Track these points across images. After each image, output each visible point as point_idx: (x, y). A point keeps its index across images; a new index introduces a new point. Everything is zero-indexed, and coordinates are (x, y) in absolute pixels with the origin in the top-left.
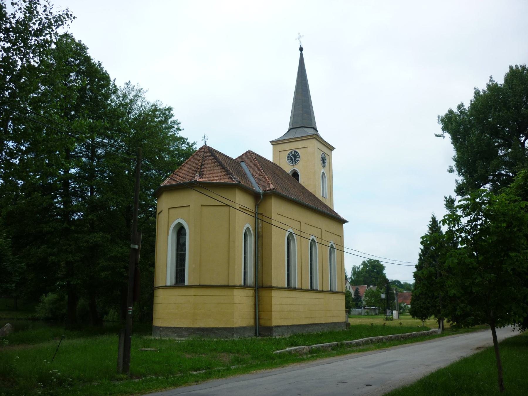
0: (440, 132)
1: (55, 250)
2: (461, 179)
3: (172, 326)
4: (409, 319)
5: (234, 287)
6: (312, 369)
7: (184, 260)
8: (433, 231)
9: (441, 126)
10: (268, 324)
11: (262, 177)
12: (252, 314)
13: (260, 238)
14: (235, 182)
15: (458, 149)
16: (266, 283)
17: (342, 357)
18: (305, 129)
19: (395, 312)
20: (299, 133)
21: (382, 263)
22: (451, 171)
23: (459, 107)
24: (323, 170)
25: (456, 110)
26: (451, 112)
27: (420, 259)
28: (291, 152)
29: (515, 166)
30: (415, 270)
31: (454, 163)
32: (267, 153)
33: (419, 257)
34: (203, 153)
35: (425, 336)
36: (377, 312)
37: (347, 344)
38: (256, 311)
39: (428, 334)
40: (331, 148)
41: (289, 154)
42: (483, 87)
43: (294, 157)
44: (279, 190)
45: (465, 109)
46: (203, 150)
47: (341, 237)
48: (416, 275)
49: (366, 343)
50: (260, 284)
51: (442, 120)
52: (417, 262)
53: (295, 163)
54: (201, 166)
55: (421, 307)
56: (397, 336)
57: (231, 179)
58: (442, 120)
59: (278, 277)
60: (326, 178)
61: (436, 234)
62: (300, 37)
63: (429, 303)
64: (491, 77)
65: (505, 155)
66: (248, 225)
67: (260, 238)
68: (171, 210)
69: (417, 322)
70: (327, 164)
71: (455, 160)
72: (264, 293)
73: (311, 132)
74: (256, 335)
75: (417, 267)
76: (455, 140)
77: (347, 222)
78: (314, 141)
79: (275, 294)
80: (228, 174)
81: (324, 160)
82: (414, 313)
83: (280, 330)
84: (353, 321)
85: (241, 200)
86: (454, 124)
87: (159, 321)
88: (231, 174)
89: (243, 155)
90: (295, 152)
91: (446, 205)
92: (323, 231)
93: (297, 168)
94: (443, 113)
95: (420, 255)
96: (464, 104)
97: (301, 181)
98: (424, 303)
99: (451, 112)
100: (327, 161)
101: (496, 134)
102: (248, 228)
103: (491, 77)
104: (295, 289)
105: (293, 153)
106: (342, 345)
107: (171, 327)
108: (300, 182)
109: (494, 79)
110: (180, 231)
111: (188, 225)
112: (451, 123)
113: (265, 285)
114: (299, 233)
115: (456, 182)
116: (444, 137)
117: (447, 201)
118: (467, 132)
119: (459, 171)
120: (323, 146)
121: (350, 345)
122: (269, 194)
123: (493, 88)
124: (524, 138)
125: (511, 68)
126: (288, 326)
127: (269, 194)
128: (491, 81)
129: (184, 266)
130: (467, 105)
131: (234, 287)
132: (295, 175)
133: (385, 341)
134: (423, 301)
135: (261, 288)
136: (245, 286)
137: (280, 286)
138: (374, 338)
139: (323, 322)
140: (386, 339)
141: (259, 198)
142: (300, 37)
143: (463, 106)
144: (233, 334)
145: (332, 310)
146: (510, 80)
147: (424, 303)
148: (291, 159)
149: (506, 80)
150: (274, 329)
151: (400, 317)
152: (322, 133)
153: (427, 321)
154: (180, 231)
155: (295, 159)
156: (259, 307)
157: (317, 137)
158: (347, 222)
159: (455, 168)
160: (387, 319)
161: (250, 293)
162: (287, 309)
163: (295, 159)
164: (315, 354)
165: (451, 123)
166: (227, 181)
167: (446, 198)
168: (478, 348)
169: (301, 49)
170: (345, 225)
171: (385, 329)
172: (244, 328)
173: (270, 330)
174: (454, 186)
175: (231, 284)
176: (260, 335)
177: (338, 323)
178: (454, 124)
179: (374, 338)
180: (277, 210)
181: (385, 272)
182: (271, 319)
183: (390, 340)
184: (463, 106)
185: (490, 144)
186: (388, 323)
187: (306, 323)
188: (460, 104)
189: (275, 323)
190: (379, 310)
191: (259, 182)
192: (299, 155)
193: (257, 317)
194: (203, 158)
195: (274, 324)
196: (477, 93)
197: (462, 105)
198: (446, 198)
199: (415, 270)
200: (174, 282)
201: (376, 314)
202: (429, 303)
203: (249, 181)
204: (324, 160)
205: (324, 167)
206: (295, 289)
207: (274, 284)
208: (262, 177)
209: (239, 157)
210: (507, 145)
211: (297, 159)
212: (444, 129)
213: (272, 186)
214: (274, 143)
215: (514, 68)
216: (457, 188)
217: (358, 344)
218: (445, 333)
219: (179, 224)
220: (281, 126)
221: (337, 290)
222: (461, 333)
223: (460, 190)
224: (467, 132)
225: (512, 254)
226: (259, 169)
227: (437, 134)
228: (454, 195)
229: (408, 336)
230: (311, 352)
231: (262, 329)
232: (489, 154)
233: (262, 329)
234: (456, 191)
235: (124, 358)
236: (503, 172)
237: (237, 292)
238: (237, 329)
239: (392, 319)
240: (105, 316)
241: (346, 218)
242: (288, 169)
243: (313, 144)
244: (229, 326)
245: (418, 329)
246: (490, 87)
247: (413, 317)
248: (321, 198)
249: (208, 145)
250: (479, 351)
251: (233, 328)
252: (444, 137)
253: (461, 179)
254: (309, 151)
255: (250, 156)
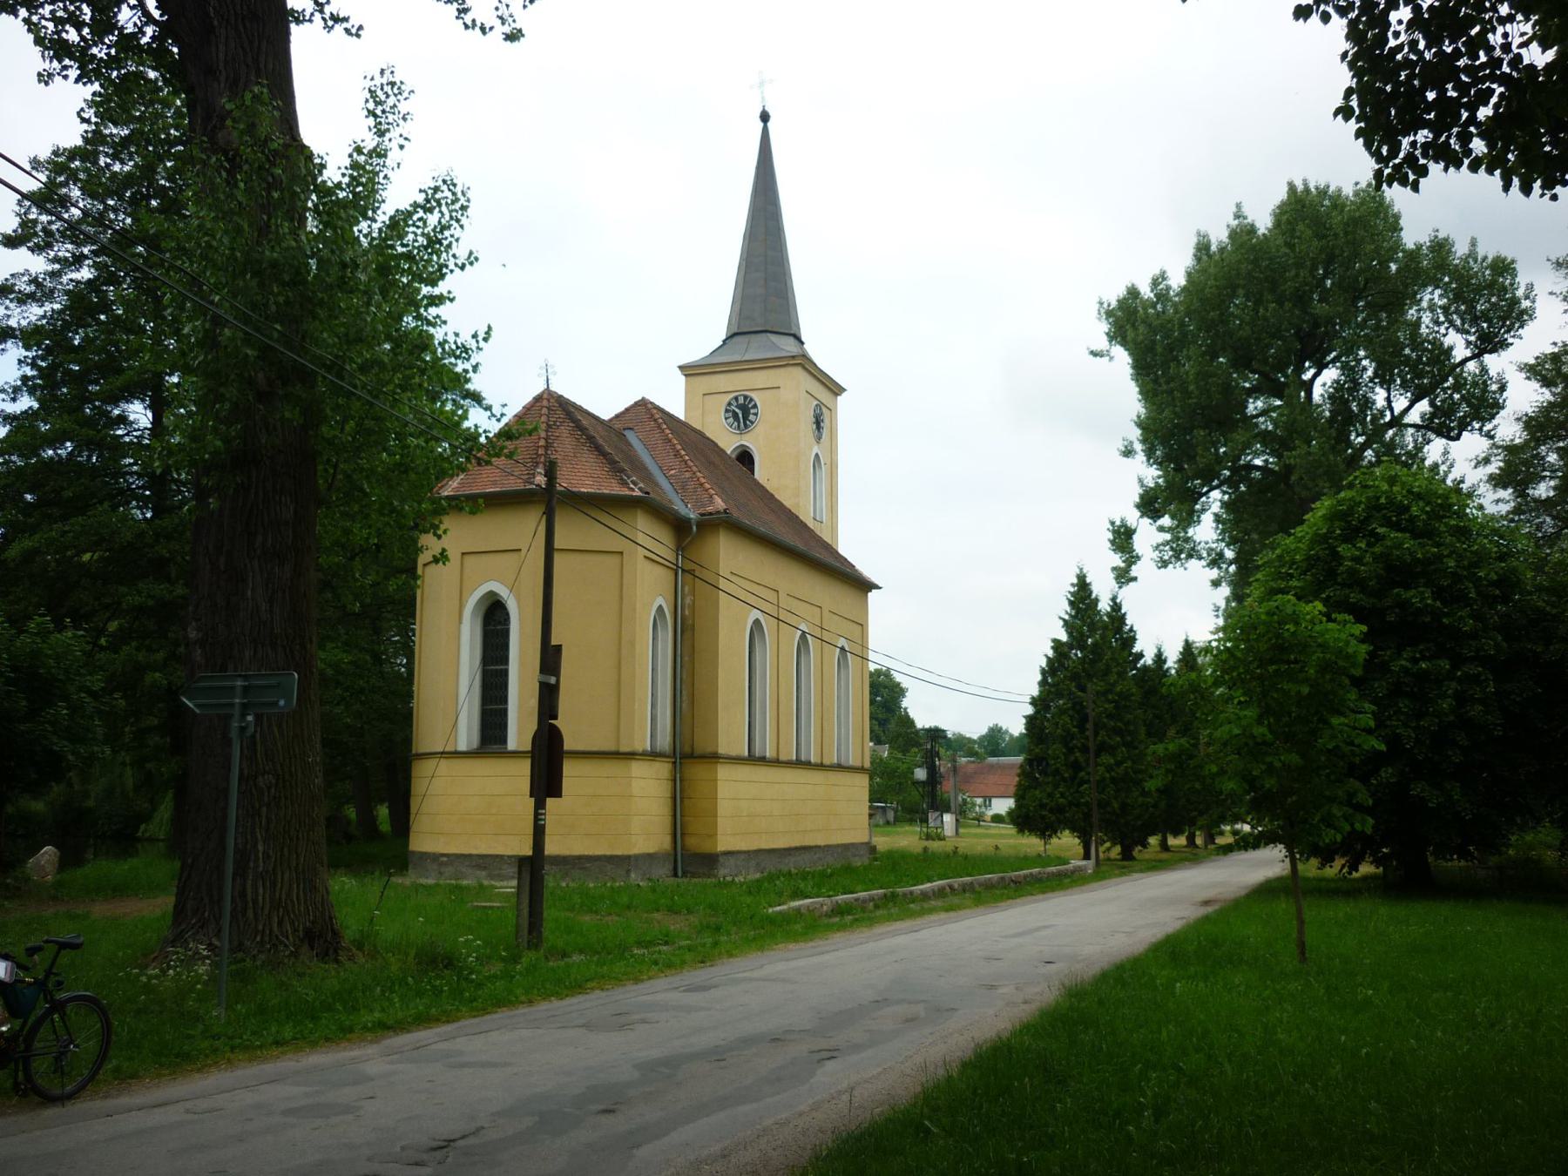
0: (1102, 343)
1: (160, 656)
2: (1153, 475)
3: (474, 852)
4: (1011, 836)
5: (631, 756)
6: (885, 943)
7: (504, 686)
8: (1078, 610)
9: (1104, 327)
10: (706, 847)
11: (688, 475)
12: (668, 820)
13: (689, 635)
14: (637, 493)
15: (1147, 394)
16: (702, 746)
17: (981, 909)
18: (773, 338)
19: (947, 818)
20: (755, 349)
21: (898, 678)
22: (1128, 453)
23: (1155, 283)
24: (816, 450)
25: (1146, 292)
26: (1133, 292)
27: (1043, 683)
28: (736, 398)
29: (1290, 449)
30: (1030, 710)
31: (1136, 433)
32: (673, 399)
33: (1039, 677)
34: (545, 411)
35: (1059, 880)
36: (891, 815)
37: (905, 895)
38: (675, 816)
39: (1060, 876)
40: (836, 389)
41: (729, 404)
42: (1219, 236)
43: (742, 412)
44: (736, 514)
45: (1168, 288)
46: (545, 403)
47: (862, 626)
48: (1030, 721)
49: (940, 893)
50: (687, 749)
51: (1109, 314)
52: (1035, 691)
53: (746, 426)
54: (546, 448)
55: (1042, 806)
56: (1003, 878)
57: (624, 484)
58: (1109, 314)
59: (730, 736)
60: (824, 467)
61: (1193, 675)
62: (762, 84)
63: (1062, 795)
64: (1238, 206)
65: (1264, 413)
66: (660, 601)
67: (689, 635)
68: (469, 560)
69: (1031, 843)
70: (825, 432)
71: (1140, 424)
72: (697, 771)
73: (789, 346)
74: (676, 875)
75: (1034, 702)
76: (1144, 370)
77: (878, 587)
78: (798, 371)
79: (724, 772)
80: (616, 470)
81: (818, 423)
82: (1022, 820)
83: (732, 861)
84: (883, 842)
85: (649, 535)
86: (1142, 329)
87: (423, 840)
88: (622, 471)
89: (627, 410)
90: (746, 397)
91: (1113, 542)
92: (826, 613)
93: (748, 441)
94: (1114, 294)
95: (1043, 672)
96: (1169, 274)
97: (760, 474)
98: (1050, 795)
99: (1133, 292)
100: (826, 425)
101: (1243, 362)
102: (660, 608)
103: (1238, 206)
104: (763, 760)
105: (741, 400)
106: (894, 896)
107: (470, 856)
108: (757, 476)
109: (1246, 210)
110: (494, 614)
111: (518, 600)
112: (1132, 322)
113: (698, 751)
114: (817, 632)
115: (1140, 481)
116: (1111, 358)
117: (1114, 532)
118: (1172, 352)
119: (1150, 453)
120: (817, 384)
121: (911, 898)
122: (712, 524)
123: (1243, 234)
124: (1312, 371)
125: (1292, 187)
126: (747, 852)
127: (712, 524)
128: (1237, 216)
129: (505, 700)
130: (1177, 280)
131: (631, 756)
132: (745, 458)
133: (977, 888)
134: (1049, 790)
135: (688, 756)
136: (653, 755)
137: (733, 753)
138: (956, 882)
139: (821, 843)
140: (980, 885)
141: (680, 528)
142: (762, 84)
143: (1164, 279)
144: (628, 872)
145: (840, 813)
146: (1289, 222)
147: (1050, 795)
148: (735, 416)
149: (1278, 223)
150: (721, 859)
151: (961, 831)
152: (813, 348)
153: (1054, 840)
154: (494, 614)
155: (745, 418)
156: (684, 805)
157: (804, 362)
158: (878, 587)
159: (1138, 447)
160: (928, 837)
161: (662, 769)
162: (754, 811)
163: (745, 418)
164: (848, 917)
165: (1132, 322)
166: (612, 488)
167: (1113, 523)
168: (1206, 903)
169: (765, 117)
170: (872, 595)
171: (925, 864)
172: (650, 855)
173: (710, 861)
174: (1135, 494)
175: (623, 749)
176: (685, 874)
177: (853, 845)
178: (1142, 329)
179: (956, 882)
180: (731, 559)
181: (905, 703)
182: (713, 835)
183: (989, 886)
184: (1164, 279)
185: (1228, 389)
186: (935, 845)
187: (786, 845)
188: (1157, 272)
189: (724, 843)
190: (896, 811)
191: (681, 488)
192: (755, 406)
193: (678, 829)
194: (549, 426)
195: (721, 848)
196: (1203, 248)
197: (1163, 276)
198: (1113, 523)
199: (1030, 710)
200: (475, 743)
201: (888, 823)
202: (1062, 795)
203: (657, 484)
204: (818, 423)
205: (819, 439)
206: (763, 760)
207: (722, 750)
208: (688, 475)
209: (617, 416)
210: (1269, 387)
211: (752, 417)
212: (1112, 337)
213: (719, 504)
214: (689, 370)
215: (1300, 187)
216: (1142, 497)
217: (925, 896)
218: (1103, 871)
219: (492, 594)
220: (708, 328)
221: (851, 763)
222: (1141, 871)
223: (1150, 505)
224: (1172, 352)
225: (1335, 721)
226: (677, 454)
227: (1094, 348)
228: (1133, 517)
229: (1025, 877)
230: (839, 911)
231: (690, 858)
232: (1224, 415)
233: (690, 858)
234: (1138, 506)
235: (531, 915)
236: (1258, 462)
237: (638, 769)
238: (637, 857)
239: (941, 838)
240: (143, 827)
241: (875, 579)
242: (729, 442)
243: (793, 382)
244: (619, 852)
245: (1040, 860)
246: (1234, 234)
247: (1021, 830)
248: (811, 524)
249: (552, 388)
250: (1210, 909)
251: (629, 857)
252: (1111, 358)
253: (1153, 475)
254: (781, 397)
255: (644, 411)
